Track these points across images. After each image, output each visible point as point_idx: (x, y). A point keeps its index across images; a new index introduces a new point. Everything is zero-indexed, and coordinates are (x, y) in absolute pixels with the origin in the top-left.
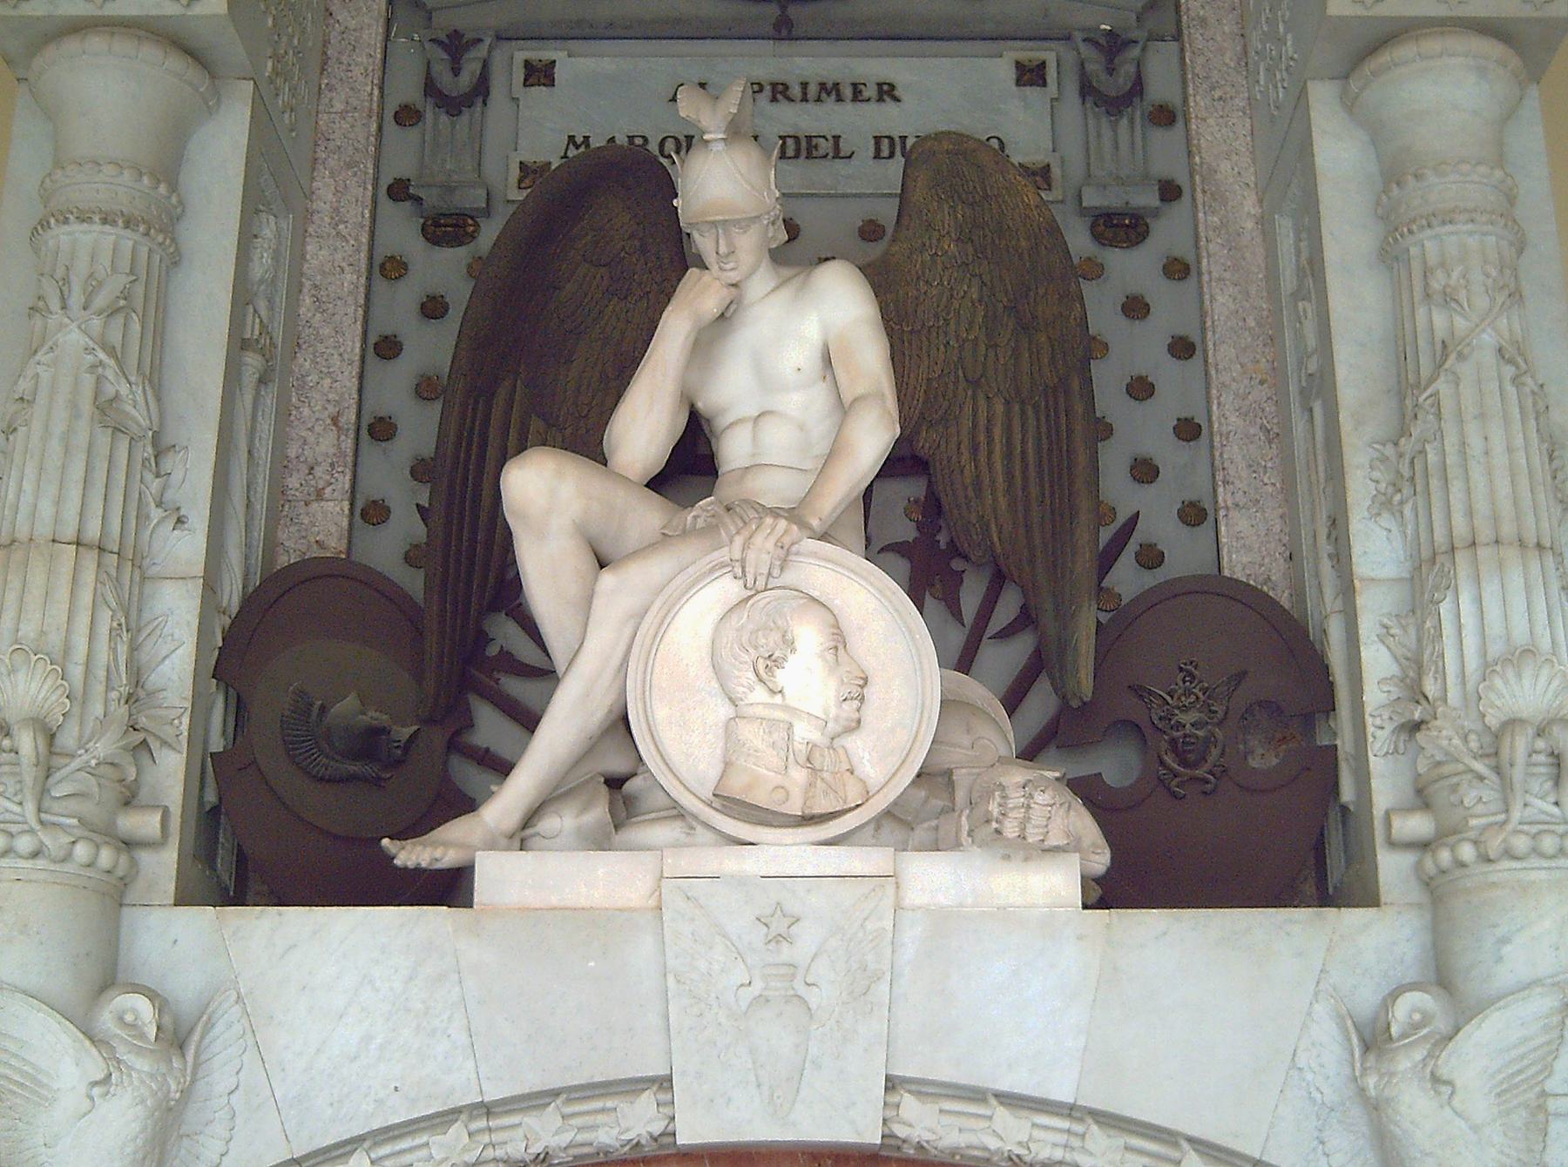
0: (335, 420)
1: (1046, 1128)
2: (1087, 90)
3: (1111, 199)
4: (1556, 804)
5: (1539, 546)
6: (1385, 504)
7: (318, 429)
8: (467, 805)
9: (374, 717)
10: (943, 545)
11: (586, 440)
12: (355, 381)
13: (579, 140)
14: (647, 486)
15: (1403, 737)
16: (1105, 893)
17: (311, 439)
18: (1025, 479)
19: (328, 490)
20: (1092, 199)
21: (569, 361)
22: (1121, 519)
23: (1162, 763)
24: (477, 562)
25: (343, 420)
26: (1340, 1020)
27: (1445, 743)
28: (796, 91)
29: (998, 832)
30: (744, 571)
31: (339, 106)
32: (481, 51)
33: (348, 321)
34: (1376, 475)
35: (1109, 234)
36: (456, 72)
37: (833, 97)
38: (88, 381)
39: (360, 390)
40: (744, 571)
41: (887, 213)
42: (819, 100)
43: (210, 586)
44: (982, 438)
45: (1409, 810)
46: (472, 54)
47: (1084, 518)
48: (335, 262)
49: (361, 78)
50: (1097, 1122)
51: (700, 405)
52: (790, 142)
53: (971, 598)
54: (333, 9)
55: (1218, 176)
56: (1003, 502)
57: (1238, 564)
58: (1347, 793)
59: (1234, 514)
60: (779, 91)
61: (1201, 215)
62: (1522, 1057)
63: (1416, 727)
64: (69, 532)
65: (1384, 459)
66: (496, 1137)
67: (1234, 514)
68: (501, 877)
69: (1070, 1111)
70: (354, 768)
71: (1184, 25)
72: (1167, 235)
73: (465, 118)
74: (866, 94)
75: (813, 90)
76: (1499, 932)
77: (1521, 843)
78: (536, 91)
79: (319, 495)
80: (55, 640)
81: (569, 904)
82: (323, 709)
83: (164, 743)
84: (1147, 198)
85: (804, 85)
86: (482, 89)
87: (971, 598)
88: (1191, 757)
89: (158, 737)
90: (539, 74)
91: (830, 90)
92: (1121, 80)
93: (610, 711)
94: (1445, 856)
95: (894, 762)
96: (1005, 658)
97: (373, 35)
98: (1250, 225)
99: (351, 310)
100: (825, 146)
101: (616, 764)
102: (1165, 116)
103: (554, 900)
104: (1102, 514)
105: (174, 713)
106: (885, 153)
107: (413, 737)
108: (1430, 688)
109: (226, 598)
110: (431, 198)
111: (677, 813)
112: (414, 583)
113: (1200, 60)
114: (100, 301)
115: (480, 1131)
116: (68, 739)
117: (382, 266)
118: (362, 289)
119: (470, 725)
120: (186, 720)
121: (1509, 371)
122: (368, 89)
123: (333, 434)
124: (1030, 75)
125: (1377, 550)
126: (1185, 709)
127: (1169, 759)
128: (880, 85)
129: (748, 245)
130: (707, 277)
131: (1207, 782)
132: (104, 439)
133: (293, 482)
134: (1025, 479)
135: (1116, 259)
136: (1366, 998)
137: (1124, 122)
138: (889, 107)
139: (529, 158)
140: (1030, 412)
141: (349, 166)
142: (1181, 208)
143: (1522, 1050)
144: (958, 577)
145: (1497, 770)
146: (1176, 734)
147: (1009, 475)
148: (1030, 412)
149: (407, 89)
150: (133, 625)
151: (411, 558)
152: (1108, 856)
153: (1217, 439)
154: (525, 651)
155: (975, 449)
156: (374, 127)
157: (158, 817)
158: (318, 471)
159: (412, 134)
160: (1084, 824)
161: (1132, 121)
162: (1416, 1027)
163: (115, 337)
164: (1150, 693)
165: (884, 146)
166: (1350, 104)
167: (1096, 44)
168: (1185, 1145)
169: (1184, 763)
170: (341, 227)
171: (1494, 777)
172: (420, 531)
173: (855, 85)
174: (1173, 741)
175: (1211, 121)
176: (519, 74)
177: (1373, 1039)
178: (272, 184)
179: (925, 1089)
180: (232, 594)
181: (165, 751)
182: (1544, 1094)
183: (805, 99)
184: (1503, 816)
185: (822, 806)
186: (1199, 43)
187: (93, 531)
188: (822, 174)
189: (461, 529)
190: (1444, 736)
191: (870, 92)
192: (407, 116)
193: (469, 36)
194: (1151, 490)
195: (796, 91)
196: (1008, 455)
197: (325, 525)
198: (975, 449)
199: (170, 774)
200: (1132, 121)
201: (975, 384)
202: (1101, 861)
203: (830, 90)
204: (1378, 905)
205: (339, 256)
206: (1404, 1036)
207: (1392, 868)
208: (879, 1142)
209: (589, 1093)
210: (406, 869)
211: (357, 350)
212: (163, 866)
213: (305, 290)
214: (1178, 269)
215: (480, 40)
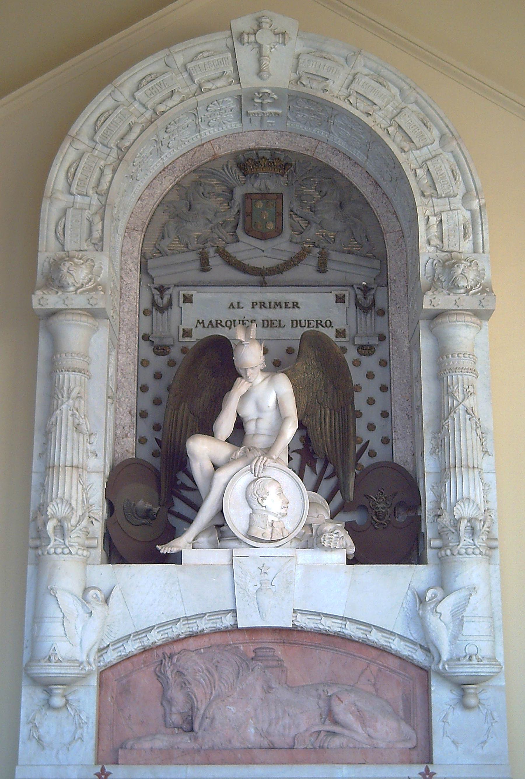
0: (130, 413)
1: (335, 623)
2: (357, 304)
3: (364, 342)
4: (473, 540)
5: (474, 467)
6: (433, 452)
9: (148, 506)
10: (311, 451)
12: (136, 400)
13: (201, 321)
14: (192, 303)
15: (436, 518)
17: (123, 418)
18: (335, 433)
19: (129, 434)
20: (358, 341)
21: (201, 396)
22: (364, 442)
23: (372, 518)
24: (177, 461)
25: (132, 412)
26: (413, 594)
27: (444, 523)
28: (267, 305)
31: (126, 310)
33: (132, 381)
34: (432, 442)
35: (363, 352)
37: (279, 306)
41: (296, 345)
42: (274, 308)
45: (436, 538)
46: (167, 292)
47: (352, 442)
49: (133, 300)
50: (349, 621)
52: (265, 322)
53: (319, 467)
54: (123, 276)
55: (397, 333)
56: (329, 440)
57: (397, 459)
58: (423, 531)
60: (262, 305)
61: (391, 346)
62: (459, 607)
63: (439, 516)
64: (68, 463)
65: (435, 438)
66: (190, 625)
67: (397, 441)
68: (189, 556)
69: (342, 618)
70: (144, 521)
71: (389, 282)
72: (380, 353)
74: (289, 306)
75: (273, 304)
76: (456, 574)
77: (463, 551)
79: (126, 436)
82: (134, 505)
84: (374, 341)
85: (270, 303)
86: (170, 303)
87: (319, 467)
88: (381, 517)
90: (188, 299)
91: (278, 305)
92: (368, 302)
94: (443, 552)
95: (296, 524)
96: (327, 485)
98: (406, 350)
100: (276, 323)
101: (219, 523)
102: (382, 313)
104: (358, 440)
106: (295, 326)
108: (442, 505)
110: (156, 341)
111: (237, 539)
113: (393, 294)
115: (186, 624)
117: (142, 363)
118: (136, 371)
119: (173, 505)
121: (468, 416)
122: (136, 304)
124: (340, 299)
125: (430, 464)
126: (379, 503)
128: (293, 303)
129: (258, 370)
130: (243, 381)
131: (384, 525)
133: (118, 432)
134: (335, 433)
135: (364, 360)
136: (422, 587)
137: (369, 315)
138: (296, 310)
139: (185, 327)
140: (337, 414)
141: (130, 330)
142: (385, 344)
143: (459, 605)
144: (315, 460)
145: (456, 530)
147: (331, 433)
148: (337, 414)
149: (146, 304)
151: (155, 454)
152: (354, 550)
153: (393, 418)
154: (189, 483)
155: (321, 423)
157: (96, 541)
160: (349, 541)
162: (433, 598)
163: (77, 405)
164: (370, 497)
165: (296, 323)
166: (431, 330)
167: (361, 289)
168: (373, 627)
169: (379, 519)
170: (129, 350)
171: (456, 533)
173: (286, 303)
174: (376, 512)
175: (396, 315)
176: (182, 300)
177: (421, 599)
179: (304, 612)
182: (463, 616)
183: (270, 308)
184: (457, 543)
186: (393, 289)
188: (276, 332)
190: (446, 519)
191: (290, 305)
192: (146, 312)
193: (166, 287)
195: (267, 305)
198: (321, 423)
201: (321, 404)
202: (352, 550)
203: (278, 305)
204: (427, 564)
205: (129, 359)
206: (429, 601)
207: (430, 553)
208: (291, 626)
209: (213, 614)
211: (136, 390)
213: (119, 371)
214: (383, 363)
215: (169, 288)
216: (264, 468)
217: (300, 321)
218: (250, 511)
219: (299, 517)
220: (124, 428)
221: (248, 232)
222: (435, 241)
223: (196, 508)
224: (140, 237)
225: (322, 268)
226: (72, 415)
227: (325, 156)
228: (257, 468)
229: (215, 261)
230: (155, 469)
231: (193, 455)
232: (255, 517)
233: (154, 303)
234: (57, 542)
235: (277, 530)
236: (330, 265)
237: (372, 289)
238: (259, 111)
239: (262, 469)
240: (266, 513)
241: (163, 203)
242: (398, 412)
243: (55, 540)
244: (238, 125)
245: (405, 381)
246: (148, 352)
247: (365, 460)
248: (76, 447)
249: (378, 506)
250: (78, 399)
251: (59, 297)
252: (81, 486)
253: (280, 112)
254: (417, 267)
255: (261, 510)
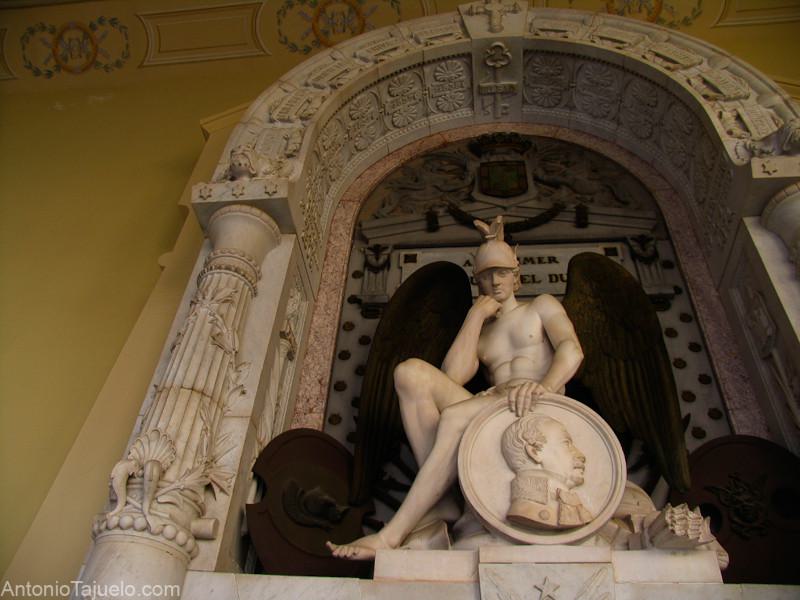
0: (320, 382)
7: (313, 385)
8: (377, 527)
11: (438, 360)
16: (730, 576)
17: (309, 388)
25: (323, 382)
29: (673, 531)
30: (517, 408)
31: (330, 271)
32: (388, 251)
36: (377, 259)
38: (208, 326)
39: (332, 371)
40: (517, 408)
43: (254, 423)
44: (615, 377)
48: (325, 324)
51: (485, 358)
56: (629, 403)
59: (736, 412)
64: (188, 384)
67: (736, 412)
70: (316, 521)
73: (380, 274)
78: (409, 265)
79: (311, 411)
80: (171, 431)
81: (426, 577)
82: (303, 492)
83: (222, 490)
86: (387, 264)
89: (219, 486)
93: (448, 480)
95: (602, 503)
97: (346, 247)
99: (330, 340)
103: (418, 576)
105: (227, 476)
107: (345, 512)
109: (263, 437)
111: (487, 529)
112: (351, 448)
114: (220, 296)
116: (170, 475)
117: (344, 327)
120: (234, 480)
123: (318, 387)
126: (739, 494)
127: (736, 519)
132: (211, 348)
133: (300, 405)
137: (653, 268)
138: (554, 265)
146: (737, 506)
147: (630, 392)
149: (358, 265)
150: (212, 435)
151: (350, 438)
156: (344, 277)
158: (311, 401)
159: (359, 281)
161: (656, 266)
166: (764, 224)
172: (353, 426)
176: (402, 259)
178: (298, 277)
180: (266, 435)
181: (222, 494)
185: (568, 521)
187: (200, 385)
189: (378, 383)
191: (546, 260)
192: (357, 275)
194: (694, 404)
196: (629, 382)
197: (314, 421)
198: (612, 382)
199: (221, 506)
200: (656, 266)
210: (338, 557)
212: (210, 551)
216: (532, 400)
217: (561, 275)
218: (511, 476)
219: (607, 488)
220: (308, 400)
221: (485, 192)
222: (738, 131)
223: (412, 472)
224: (356, 207)
225: (581, 221)
226: (211, 322)
227: (565, 135)
228: (521, 399)
229: (445, 220)
230: (349, 453)
231: (405, 388)
232: (522, 483)
233: (367, 264)
234: (128, 507)
235: (568, 510)
236: (591, 219)
237: (651, 239)
238: (491, 84)
239: (529, 401)
240: (543, 475)
241: (386, 181)
242: (726, 372)
243: (127, 503)
244: (470, 113)
245: (724, 335)
246: (353, 314)
247: (691, 444)
248: (207, 364)
249: (741, 498)
250: (227, 304)
251: (227, 186)
252: (202, 423)
253: (514, 83)
254: (722, 156)
255: (534, 470)
